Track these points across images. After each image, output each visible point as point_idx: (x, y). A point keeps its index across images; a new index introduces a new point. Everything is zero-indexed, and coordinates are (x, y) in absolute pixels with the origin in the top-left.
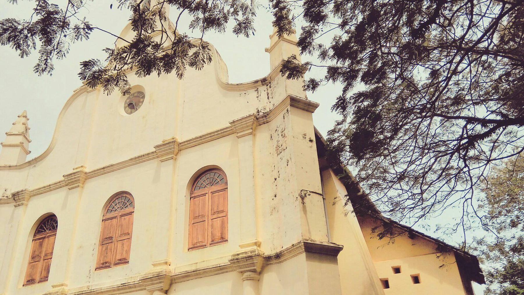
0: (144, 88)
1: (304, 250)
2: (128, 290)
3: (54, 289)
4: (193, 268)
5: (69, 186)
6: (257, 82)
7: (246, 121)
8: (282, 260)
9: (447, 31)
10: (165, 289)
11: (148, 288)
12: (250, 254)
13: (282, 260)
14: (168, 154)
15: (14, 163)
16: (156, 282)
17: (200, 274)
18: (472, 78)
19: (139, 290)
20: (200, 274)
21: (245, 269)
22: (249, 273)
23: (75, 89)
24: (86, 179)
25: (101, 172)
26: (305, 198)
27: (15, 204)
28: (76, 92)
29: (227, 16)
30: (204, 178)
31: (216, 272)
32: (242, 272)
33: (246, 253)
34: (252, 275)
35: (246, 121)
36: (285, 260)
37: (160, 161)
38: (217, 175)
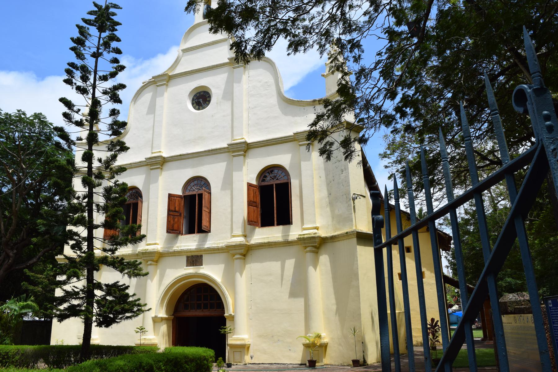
0: (210, 90)
2: (213, 252)
4: (266, 241)
6: (314, 101)
9: (305, 5)
10: (245, 253)
11: (231, 252)
12: (313, 235)
13: (334, 241)
14: (239, 151)
16: (238, 248)
17: (271, 245)
18: (488, 162)
19: (221, 252)
20: (271, 245)
21: (309, 245)
22: (311, 248)
23: (143, 81)
26: (356, 200)
28: (145, 84)
29: (297, 39)
31: (284, 245)
33: (309, 234)
34: (314, 249)
35: (297, 136)
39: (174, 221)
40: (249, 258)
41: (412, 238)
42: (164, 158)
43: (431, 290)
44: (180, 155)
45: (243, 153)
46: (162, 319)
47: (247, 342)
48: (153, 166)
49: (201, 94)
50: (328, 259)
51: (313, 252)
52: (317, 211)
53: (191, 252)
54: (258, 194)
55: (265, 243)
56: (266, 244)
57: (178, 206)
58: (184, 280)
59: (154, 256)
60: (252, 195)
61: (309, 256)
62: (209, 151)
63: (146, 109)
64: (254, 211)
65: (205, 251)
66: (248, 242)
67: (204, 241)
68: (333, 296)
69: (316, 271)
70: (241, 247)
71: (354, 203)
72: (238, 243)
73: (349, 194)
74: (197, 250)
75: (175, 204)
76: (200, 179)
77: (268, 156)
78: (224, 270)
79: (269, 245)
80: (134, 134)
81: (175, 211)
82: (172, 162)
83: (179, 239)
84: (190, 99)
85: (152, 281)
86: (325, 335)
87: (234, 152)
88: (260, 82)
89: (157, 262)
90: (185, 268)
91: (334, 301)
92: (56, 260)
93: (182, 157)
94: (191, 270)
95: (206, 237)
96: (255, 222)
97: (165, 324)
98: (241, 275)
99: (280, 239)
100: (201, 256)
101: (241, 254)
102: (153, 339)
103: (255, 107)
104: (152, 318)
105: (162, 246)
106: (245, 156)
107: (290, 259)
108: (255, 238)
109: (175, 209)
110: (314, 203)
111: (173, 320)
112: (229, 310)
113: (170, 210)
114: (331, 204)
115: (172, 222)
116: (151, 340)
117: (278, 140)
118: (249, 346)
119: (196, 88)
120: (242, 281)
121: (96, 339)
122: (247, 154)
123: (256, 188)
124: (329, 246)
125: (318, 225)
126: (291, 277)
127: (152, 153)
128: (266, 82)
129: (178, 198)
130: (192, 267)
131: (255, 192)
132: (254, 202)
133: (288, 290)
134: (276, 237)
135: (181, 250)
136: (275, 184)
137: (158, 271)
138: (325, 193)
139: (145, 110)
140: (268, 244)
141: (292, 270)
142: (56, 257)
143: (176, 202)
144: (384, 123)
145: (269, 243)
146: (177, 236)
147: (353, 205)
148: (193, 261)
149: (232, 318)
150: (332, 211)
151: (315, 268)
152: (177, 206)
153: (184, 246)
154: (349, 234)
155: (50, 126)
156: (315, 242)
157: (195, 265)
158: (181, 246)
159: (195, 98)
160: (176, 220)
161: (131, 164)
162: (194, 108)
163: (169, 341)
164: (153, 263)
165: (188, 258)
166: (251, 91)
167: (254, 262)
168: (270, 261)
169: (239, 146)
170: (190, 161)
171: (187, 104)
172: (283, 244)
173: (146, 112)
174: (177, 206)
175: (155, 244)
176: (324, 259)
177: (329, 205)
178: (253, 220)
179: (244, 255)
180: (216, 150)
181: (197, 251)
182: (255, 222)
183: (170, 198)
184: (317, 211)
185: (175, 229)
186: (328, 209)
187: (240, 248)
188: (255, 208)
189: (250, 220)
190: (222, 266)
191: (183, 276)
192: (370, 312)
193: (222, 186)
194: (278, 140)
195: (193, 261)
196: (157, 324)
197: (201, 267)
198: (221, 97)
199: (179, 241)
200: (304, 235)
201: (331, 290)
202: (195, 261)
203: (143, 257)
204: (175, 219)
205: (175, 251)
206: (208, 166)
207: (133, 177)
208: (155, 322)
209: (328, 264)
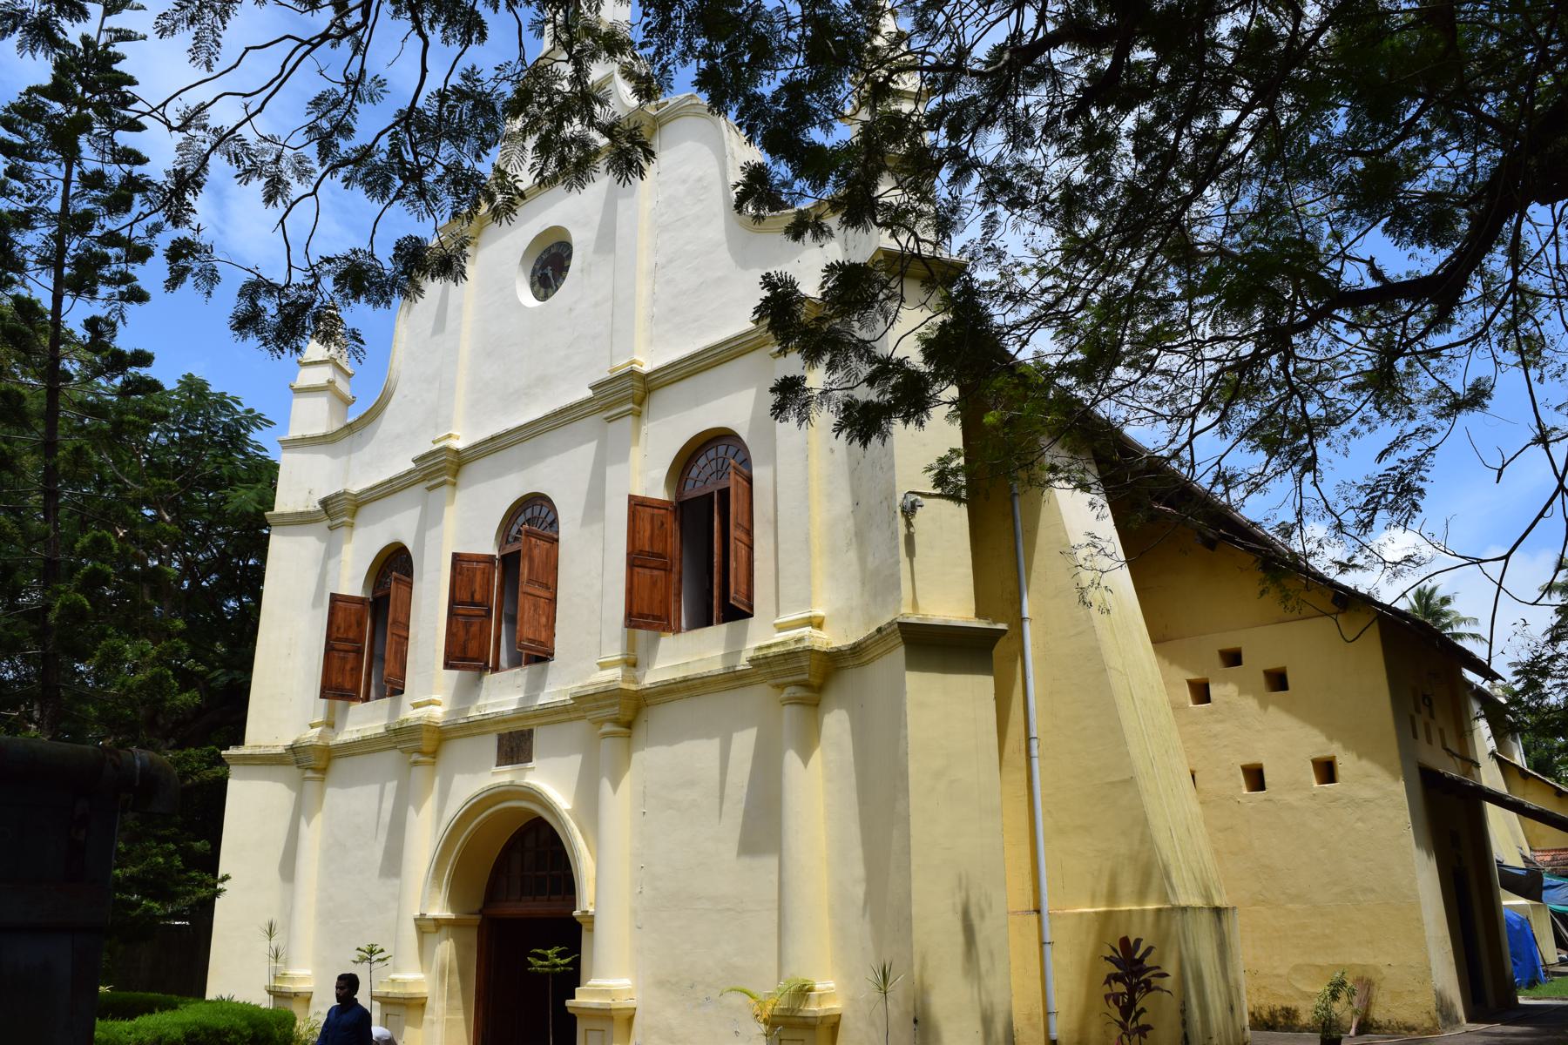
1: (900, 639)
3: (604, 673)
5: (769, 346)
7: (436, 464)
8: (863, 660)
10: (628, 718)
12: (792, 647)
13: (863, 660)
14: (620, 402)
15: (320, 430)
17: (694, 687)
20: (694, 687)
24: (358, 507)
25: (488, 447)
27: (328, 522)
30: (702, 461)
32: (777, 686)
33: (783, 643)
34: (801, 693)
36: (871, 660)
37: (606, 419)
38: (732, 450)
39: (467, 632)
40: (640, 732)
41: (1378, 634)
42: (457, 452)
43: (1359, 824)
44: (493, 439)
45: (630, 406)
46: (439, 923)
47: (621, 1002)
48: (432, 479)
49: (553, 251)
50: (847, 725)
51: (799, 702)
52: (820, 565)
53: (505, 721)
54: (673, 526)
55: (676, 682)
56: (679, 685)
57: (481, 587)
58: (490, 807)
59: (421, 739)
60: (647, 534)
61: (790, 714)
62: (556, 414)
63: (431, 323)
64: (654, 583)
65: (536, 717)
66: (636, 682)
67: (536, 686)
68: (857, 853)
69: (806, 767)
70: (610, 697)
71: (909, 524)
72: (601, 688)
73: (893, 494)
74: (521, 714)
75: (471, 581)
76: (539, 502)
77: (697, 405)
78: (580, 772)
79: (689, 689)
80: (405, 396)
81: (473, 604)
82: (480, 461)
83: (484, 685)
84: (525, 271)
85: (418, 811)
86: (832, 985)
87: (608, 407)
88: (684, 182)
89: (434, 754)
90: (495, 769)
91: (859, 871)
92: (223, 759)
93: (506, 441)
94: (505, 776)
95: (544, 673)
96: (655, 617)
97: (447, 939)
98: (615, 785)
99: (717, 667)
100: (530, 732)
101: (616, 722)
102: (417, 982)
103: (671, 261)
104: (415, 920)
105: (447, 709)
106: (639, 415)
107: (742, 729)
108: (657, 666)
109: (473, 596)
110: (807, 540)
111: (479, 927)
112: (586, 901)
113: (457, 601)
114: (860, 536)
115: (462, 633)
116: (404, 984)
117: (718, 350)
118: (631, 1013)
119: (539, 238)
120: (619, 802)
121: (303, 979)
122: (645, 409)
123: (663, 511)
124: (851, 677)
125: (819, 611)
126: (745, 790)
127: (434, 442)
128: (700, 179)
129: (482, 565)
130: (508, 768)
131: (657, 523)
132: (653, 555)
133: (736, 835)
134: (708, 659)
135: (481, 718)
136: (718, 491)
137: (437, 780)
138: (844, 502)
139: (430, 325)
140: (684, 684)
141: (747, 767)
142: (223, 752)
143: (475, 575)
144: (363, 182)
145: (685, 680)
146: (480, 678)
147: (902, 530)
148: (512, 749)
149: (591, 918)
150: (862, 560)
151: (805, 757)
152: (477, 587)
153: (493, 705)
154: (884, 633)
155: (234, 404)
156: (801, 670)
157: (515, 760)
158: (486, 706)
159: (538, 267)
160: (475, 629)
161: (391, 481)
162: (536, 296)
163: (464, 989)
164: (422, 759)
165: (501, 738)
166: (662, 215)
167: (652, 746)
168: (694, 737)
169: (618, 386)
170: (514, 452)
171: (515, 290)
172: (725, 681)
173: (431, 330)
174: (478, 588)
175: (430, 703)
176: (836, 723)
177: (854, 540)
178: (646, 612)
179: (629, 725)
180: (571, 408)
181: (519, 719)
182: (655, 617)
183: (458, 567)
184: (820, 565)
185: (470, 654)
186: (852, 555)
187: (608, 702)
188: (656, 572)
189: (635, 611)
190: (575, 761)
191: (484, 795)
192: (959, 909)
193: (585, 515)
194: (724, 348)
195: (512, 749)
196: (428, 938)
197: (530, 765)
198: (591, 248)
199: (483, 692)
200: (769, 647)
201: (854, 831)
202: (515, 749)
203: (399, 742)
204: (471, 625)
205: (471, 720)
206: (555, 458)
207: (396, 518)
208: (423, 932)
209: (847, 741)
